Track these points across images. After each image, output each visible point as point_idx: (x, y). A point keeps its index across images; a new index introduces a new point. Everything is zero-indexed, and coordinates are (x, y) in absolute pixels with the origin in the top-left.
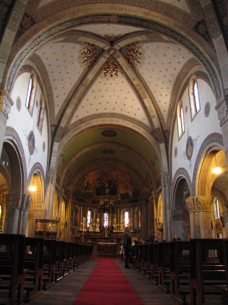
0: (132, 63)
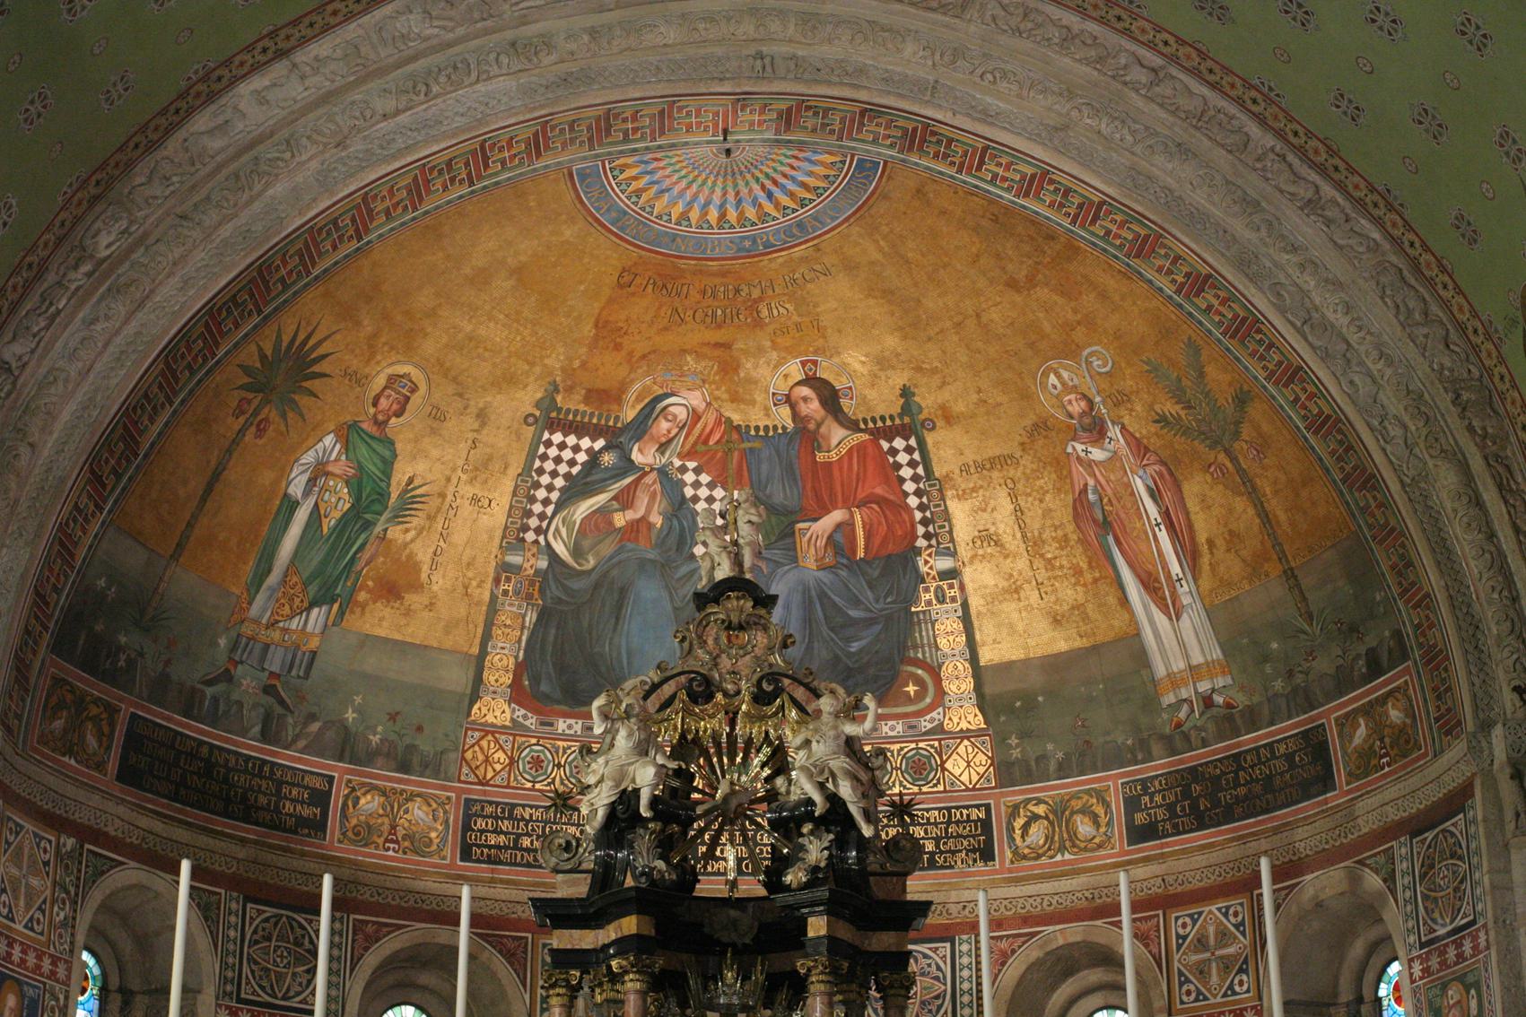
0: (1185, 700)
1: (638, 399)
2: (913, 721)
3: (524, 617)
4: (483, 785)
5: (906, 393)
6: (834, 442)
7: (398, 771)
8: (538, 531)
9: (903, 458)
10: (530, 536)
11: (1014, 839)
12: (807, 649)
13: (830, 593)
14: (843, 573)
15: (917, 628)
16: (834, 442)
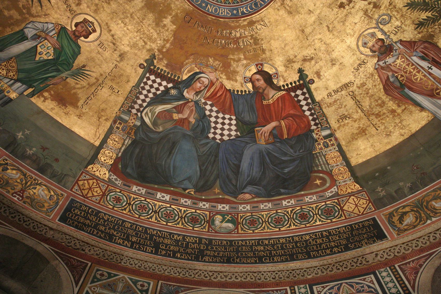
1: (189, 71)
2: (321, 194)
3: (125, 140)
4: (84, 197)
5: (300, 71)
6: (271, 96)
7: (37, 170)
8: (138, 110)
9: (301, 97)
10: (134, 111)
11: (396, 226)
12: (263, 173)
13: (272, 152)
14: (278, 145)
15: (317, 159)
16: (271, 96)
